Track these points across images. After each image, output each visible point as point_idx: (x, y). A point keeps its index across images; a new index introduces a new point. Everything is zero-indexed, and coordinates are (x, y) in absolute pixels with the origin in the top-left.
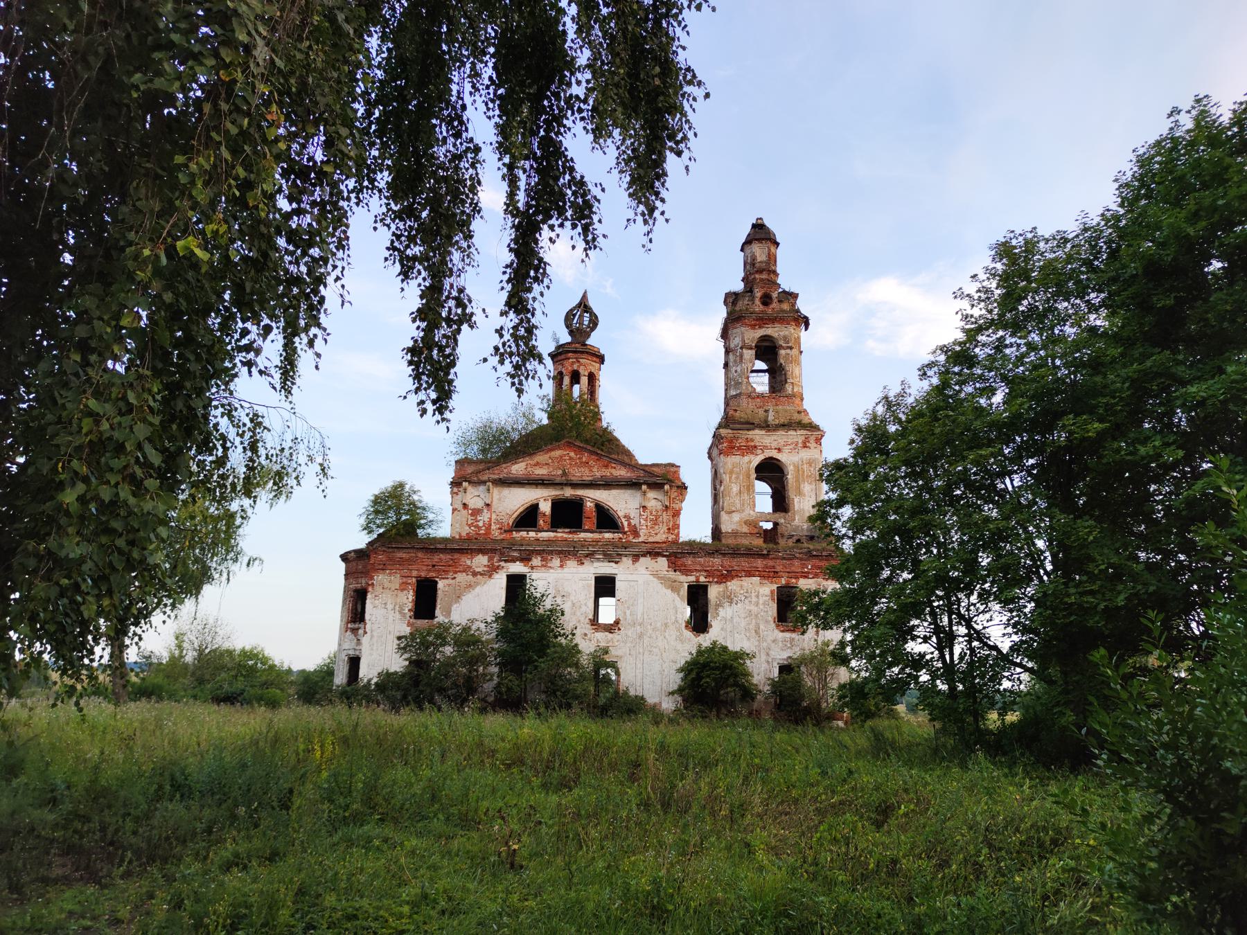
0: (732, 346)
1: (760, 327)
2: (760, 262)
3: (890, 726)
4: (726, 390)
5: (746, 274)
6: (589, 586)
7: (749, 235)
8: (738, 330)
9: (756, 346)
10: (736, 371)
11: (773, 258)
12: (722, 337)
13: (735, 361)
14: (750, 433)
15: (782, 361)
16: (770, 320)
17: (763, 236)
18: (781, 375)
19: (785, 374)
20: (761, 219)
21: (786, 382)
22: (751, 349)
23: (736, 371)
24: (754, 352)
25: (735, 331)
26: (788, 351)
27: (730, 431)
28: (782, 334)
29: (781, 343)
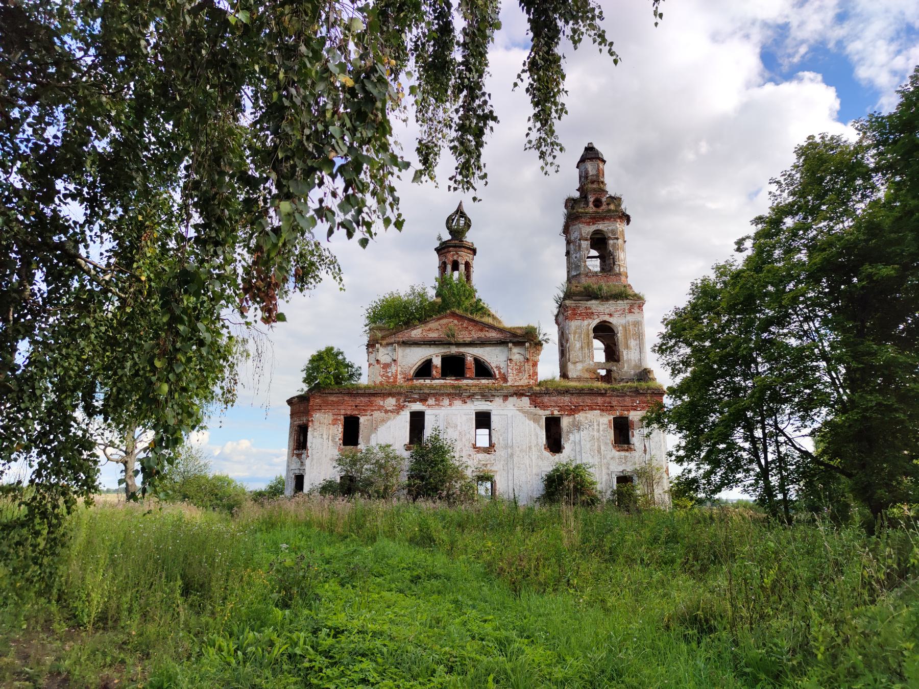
0: (572, 238)
1: (594, 224)
4: (568, 272)
12: (564, 232)
14: (589, 302)
17: (593, 156)
26: (615, 241)
29: (610, 235)
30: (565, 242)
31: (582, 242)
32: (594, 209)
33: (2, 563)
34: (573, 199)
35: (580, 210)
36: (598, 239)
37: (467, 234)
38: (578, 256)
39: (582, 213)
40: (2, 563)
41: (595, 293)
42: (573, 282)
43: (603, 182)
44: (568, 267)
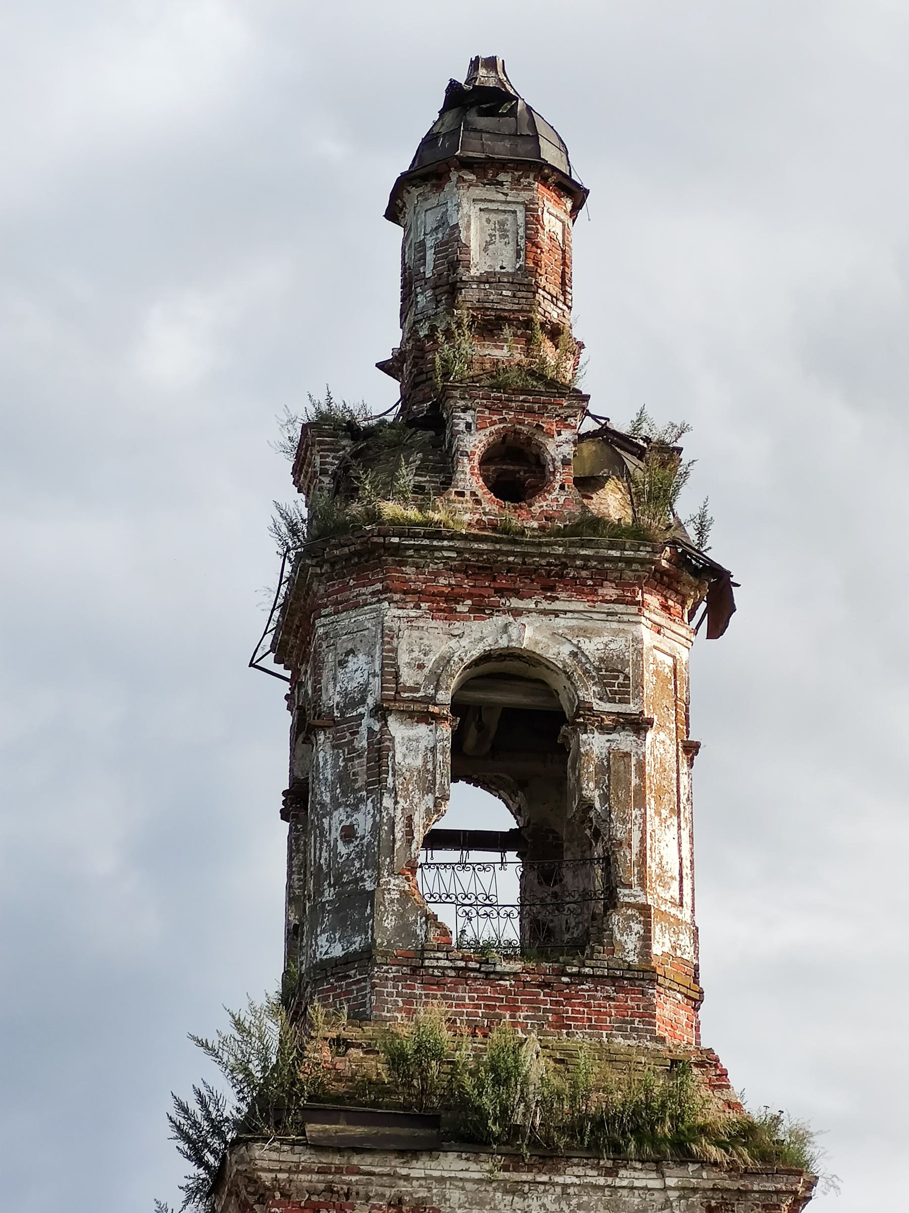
0: (332, 697)
1: (480, 610)
2: (485, 279)
3: (440, 648)
4: (294, 934)
5: (411, 334)
6: (554, 163)
7: (429, 140)
8: (364, 617)
9: (457, 707)
10: (349, 834)
11: (549, 261)
12: (281, 651)
13: (344, 779)
14: (420, 1168)
15: (591, 791)
16: (529, 572)
17: (502, 149)
18: (586, 861)
19: (608, 862)
20: (491, 63)
21: (612, 902)
22: (427, 718)
23: (349, 834)
24: (446, 731)
25: (347, 620)
26: (624, 741)
27: (306, 1158)
28: (592, 647)
29: (589, 694)
30: (287, 719)
31: (398, 729)
32: (491, 505)
33: (348, 1211)
34: (351, 429)
35: (390, 508)
36: (511, 714)
37: (624, 432)
38: (363, 822)
39: (404, 528)
40: (348, 1211)
41: (464, 1104)
42: (317, 1011)
43: (555, 332)
44: (293, 899)
